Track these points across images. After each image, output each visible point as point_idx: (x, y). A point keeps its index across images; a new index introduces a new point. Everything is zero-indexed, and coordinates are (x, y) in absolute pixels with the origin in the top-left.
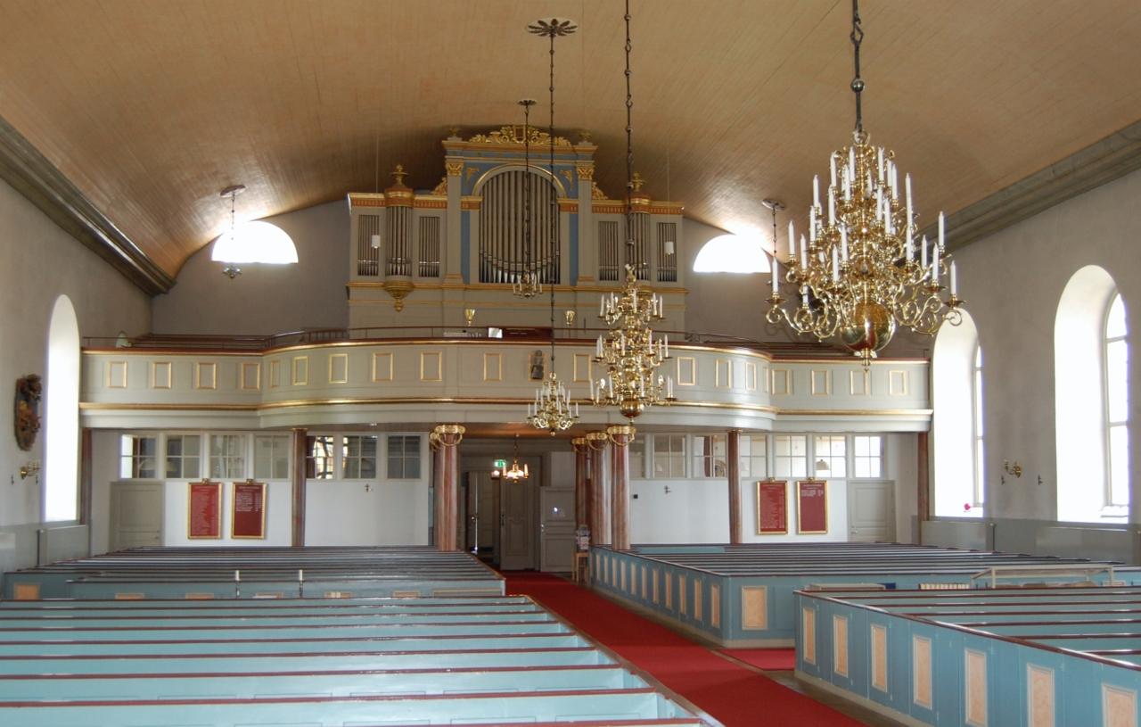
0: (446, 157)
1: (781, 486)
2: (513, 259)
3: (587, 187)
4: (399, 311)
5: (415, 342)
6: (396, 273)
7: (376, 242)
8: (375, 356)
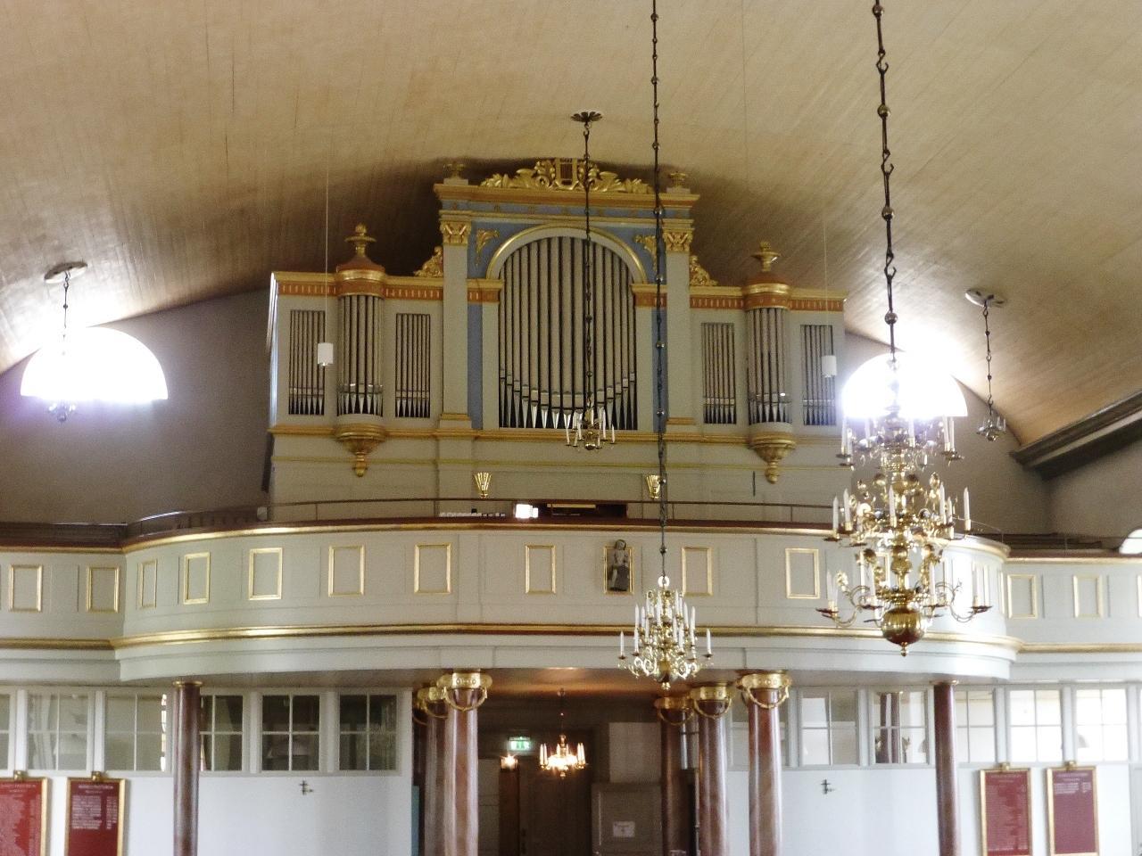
0: (441, 212)
1: (1022, 778)
2: (556, 386)
3: (679, 264)
4: (360, 476)
5: (403, 526)
6: (357, 411)
7: (325, 354)
8: (331, 552)
